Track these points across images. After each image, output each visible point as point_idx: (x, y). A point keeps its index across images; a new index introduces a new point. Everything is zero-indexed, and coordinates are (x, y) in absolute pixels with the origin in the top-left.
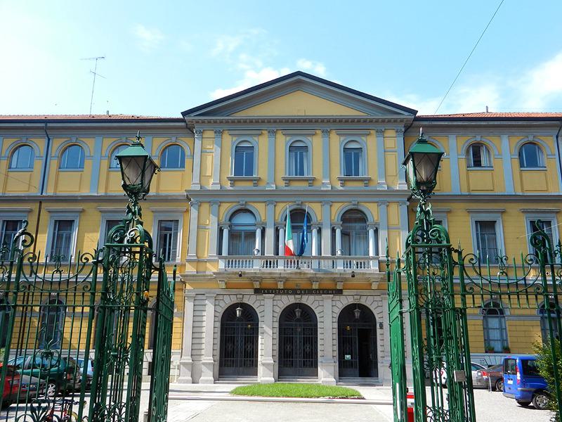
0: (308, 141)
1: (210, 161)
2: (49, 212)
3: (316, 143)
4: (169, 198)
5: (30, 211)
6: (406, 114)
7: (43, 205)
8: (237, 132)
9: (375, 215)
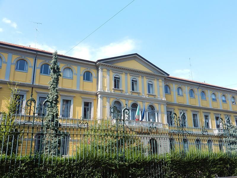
0: (226, 95)
1: (104, 81)
2: (37, 93)
3: (140, 80)
4: (89, 93)
5: (28, 91)
6: (167, 75)
7: (33, 89)
8: (133, 75)
9: (157, 108)
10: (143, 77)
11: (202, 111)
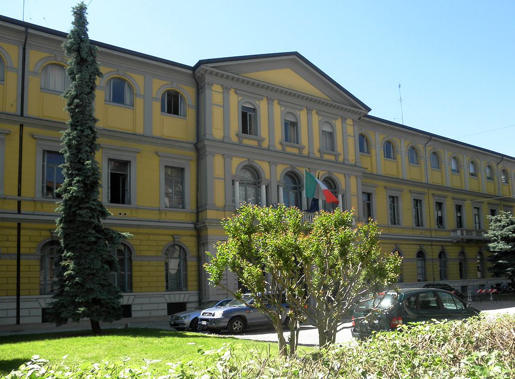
6: (364, 109)
7: (25, 128)
8: (324, 114)
10: (270, 100)
11: (431, 191)
